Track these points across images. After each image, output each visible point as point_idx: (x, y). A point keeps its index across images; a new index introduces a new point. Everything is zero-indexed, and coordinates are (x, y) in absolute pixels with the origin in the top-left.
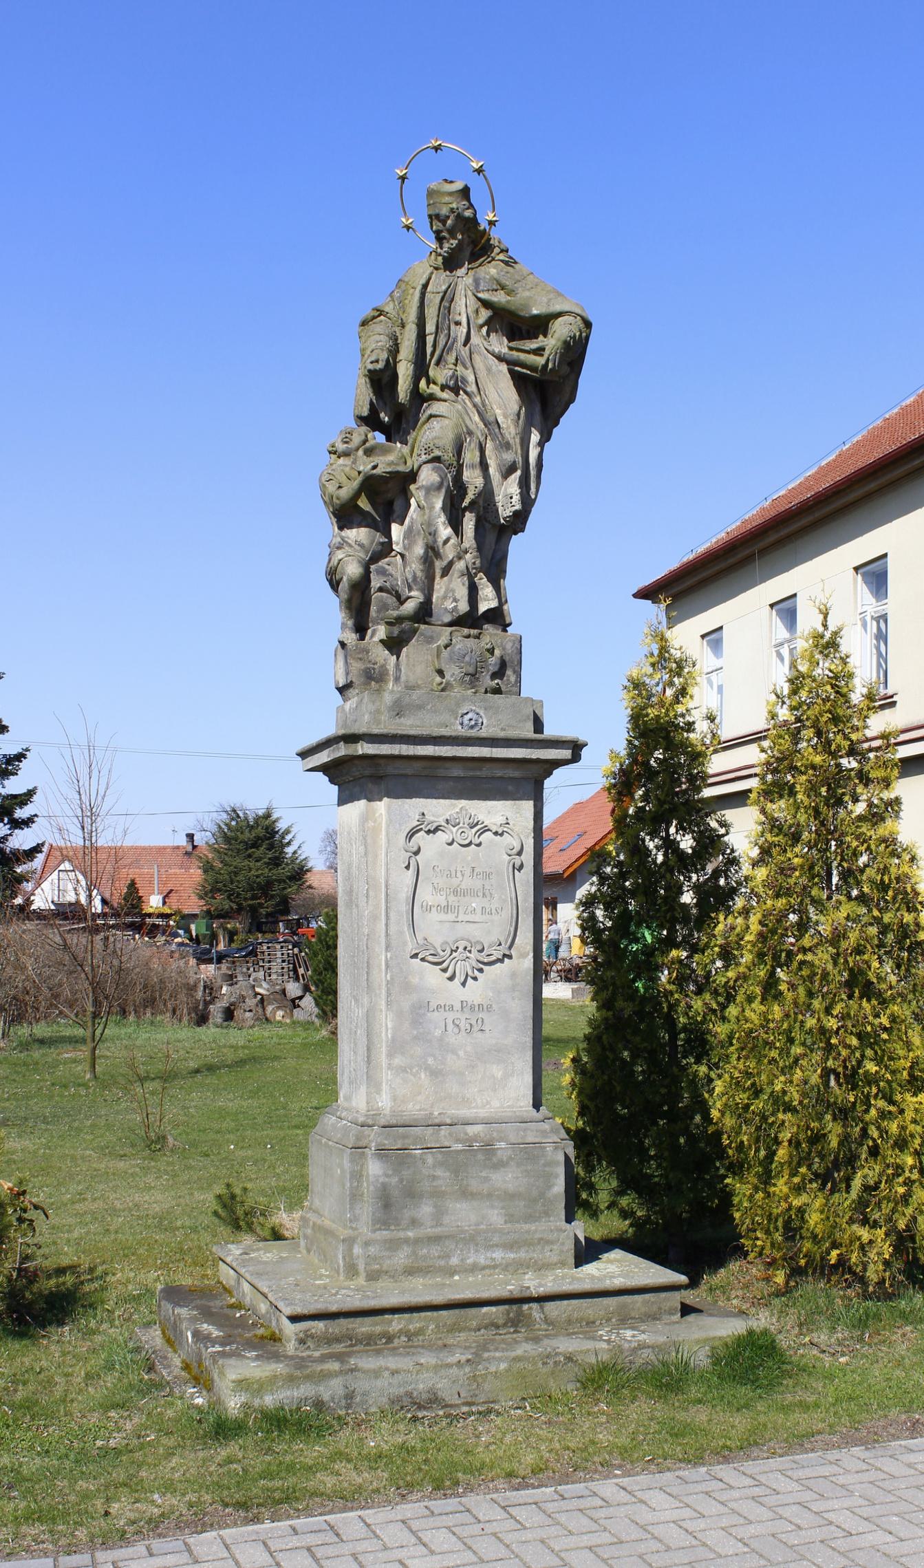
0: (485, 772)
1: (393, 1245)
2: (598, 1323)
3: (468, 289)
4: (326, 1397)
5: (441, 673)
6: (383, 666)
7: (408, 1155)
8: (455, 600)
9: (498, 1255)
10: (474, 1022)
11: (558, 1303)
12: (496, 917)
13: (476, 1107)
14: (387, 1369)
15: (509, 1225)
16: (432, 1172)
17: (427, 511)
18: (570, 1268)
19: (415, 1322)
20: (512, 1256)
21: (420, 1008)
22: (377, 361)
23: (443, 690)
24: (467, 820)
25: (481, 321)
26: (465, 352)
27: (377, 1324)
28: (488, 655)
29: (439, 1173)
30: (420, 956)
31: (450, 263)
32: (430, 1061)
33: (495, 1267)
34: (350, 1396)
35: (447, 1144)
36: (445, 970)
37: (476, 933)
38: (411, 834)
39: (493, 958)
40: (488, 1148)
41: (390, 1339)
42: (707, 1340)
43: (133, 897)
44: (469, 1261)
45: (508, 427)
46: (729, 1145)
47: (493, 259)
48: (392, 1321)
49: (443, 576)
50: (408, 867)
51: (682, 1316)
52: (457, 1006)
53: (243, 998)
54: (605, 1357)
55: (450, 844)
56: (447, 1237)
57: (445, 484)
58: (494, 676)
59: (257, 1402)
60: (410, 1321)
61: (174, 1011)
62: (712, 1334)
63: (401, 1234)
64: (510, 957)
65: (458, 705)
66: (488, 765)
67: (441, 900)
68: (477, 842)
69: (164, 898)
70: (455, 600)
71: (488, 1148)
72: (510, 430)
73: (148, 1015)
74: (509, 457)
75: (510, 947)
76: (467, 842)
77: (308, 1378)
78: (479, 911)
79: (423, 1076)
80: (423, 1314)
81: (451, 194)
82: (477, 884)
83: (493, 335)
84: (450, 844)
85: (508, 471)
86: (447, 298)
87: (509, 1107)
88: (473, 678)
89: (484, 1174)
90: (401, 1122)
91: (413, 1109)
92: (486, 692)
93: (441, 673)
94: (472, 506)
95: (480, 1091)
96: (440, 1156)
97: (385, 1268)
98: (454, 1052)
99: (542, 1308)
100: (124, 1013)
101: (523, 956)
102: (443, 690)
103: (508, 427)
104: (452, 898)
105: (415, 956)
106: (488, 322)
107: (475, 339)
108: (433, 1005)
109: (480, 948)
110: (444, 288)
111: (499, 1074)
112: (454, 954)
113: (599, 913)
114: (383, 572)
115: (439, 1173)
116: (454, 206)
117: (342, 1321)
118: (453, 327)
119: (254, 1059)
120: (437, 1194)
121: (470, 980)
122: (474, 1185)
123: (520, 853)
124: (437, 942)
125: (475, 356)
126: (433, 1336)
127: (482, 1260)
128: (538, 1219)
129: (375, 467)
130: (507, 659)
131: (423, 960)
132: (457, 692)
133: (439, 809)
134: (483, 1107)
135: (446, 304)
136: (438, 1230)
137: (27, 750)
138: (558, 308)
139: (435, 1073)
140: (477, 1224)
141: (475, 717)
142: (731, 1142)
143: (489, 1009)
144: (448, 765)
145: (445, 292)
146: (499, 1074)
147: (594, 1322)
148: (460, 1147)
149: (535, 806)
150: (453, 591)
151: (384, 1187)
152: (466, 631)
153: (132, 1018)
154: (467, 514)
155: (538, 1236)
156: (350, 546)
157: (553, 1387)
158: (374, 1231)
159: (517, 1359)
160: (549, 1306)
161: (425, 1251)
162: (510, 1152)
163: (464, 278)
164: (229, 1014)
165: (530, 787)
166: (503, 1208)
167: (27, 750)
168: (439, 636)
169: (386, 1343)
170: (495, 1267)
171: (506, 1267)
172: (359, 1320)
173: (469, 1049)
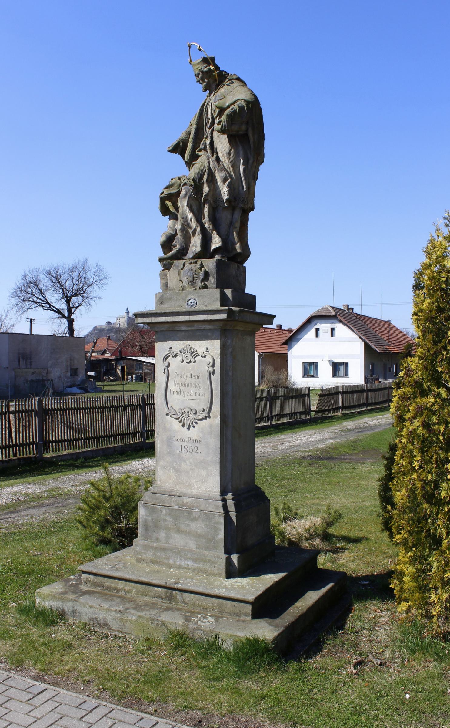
0: (196, 327)
2: (208, 610)
7: (156, 507)
9: (190, 563)
10: (193, 448)
12: (202, 398)
14: (88, 604)
15: (198, 550)
18: (223, 578)
19: (129, 586)
20: (197, 565)
21: (171, 439)
23: (183, 290)
27: (113, 583)
28: (200, 271)
30: (170, 415)
32: (175, 464)
33: (189, 569)
35: (173, 505)
37: (193, 405)
42: (232, 636)
47: (224, 85)
48: (118, 583)
49: (193, 236)
50: (164, 372)
52: (186, 440)
55: (182, 362)
57: (189, 194)
60: (126, 585)
62: (235, 634)
63: (151, 544)
64: (209, 417)
65: (186, 296)
66: (196, 324)
72: (225, 161)
75: (209, 412)
77: (60, 599)
78: (194, 394)
80: (131, 583)
81: (198, 64)
84: (182, 362)
88: (192, 282)
90: (159, 492)
95: (196, 482)
96: (168, 511)
97: (143, 558)
99: (182, 595)
101: (215, 417)
104: (182, 388)
105: (167, 414)
108: (176, 438)
109: (194, 412)
111: (205, 475)
112: (184, 415)
115: (168, 518)
117: (99, 577)
120: (167, 529)
121: (191, 428)
122: (183, 527)
123: (213, 366)
124: (177, 408)
130: (210, 272)
139: (177, 471)
140: (184, 546)
143: (200, 441)
144: (179, 325)
146: (205, 475)
147: (206, 609)
148: (177, 507)
151: (146, 520)
154: (205, 205)
155: (208, 558)
158: (142, 540)
159: (139, 617)
160: (185, 595)
161: (159, 554)
162: (199, 514)
165: (218, 333)
169: (116, 593)
170: (189, 569)
172: (106, 579)
173: (191, 461)
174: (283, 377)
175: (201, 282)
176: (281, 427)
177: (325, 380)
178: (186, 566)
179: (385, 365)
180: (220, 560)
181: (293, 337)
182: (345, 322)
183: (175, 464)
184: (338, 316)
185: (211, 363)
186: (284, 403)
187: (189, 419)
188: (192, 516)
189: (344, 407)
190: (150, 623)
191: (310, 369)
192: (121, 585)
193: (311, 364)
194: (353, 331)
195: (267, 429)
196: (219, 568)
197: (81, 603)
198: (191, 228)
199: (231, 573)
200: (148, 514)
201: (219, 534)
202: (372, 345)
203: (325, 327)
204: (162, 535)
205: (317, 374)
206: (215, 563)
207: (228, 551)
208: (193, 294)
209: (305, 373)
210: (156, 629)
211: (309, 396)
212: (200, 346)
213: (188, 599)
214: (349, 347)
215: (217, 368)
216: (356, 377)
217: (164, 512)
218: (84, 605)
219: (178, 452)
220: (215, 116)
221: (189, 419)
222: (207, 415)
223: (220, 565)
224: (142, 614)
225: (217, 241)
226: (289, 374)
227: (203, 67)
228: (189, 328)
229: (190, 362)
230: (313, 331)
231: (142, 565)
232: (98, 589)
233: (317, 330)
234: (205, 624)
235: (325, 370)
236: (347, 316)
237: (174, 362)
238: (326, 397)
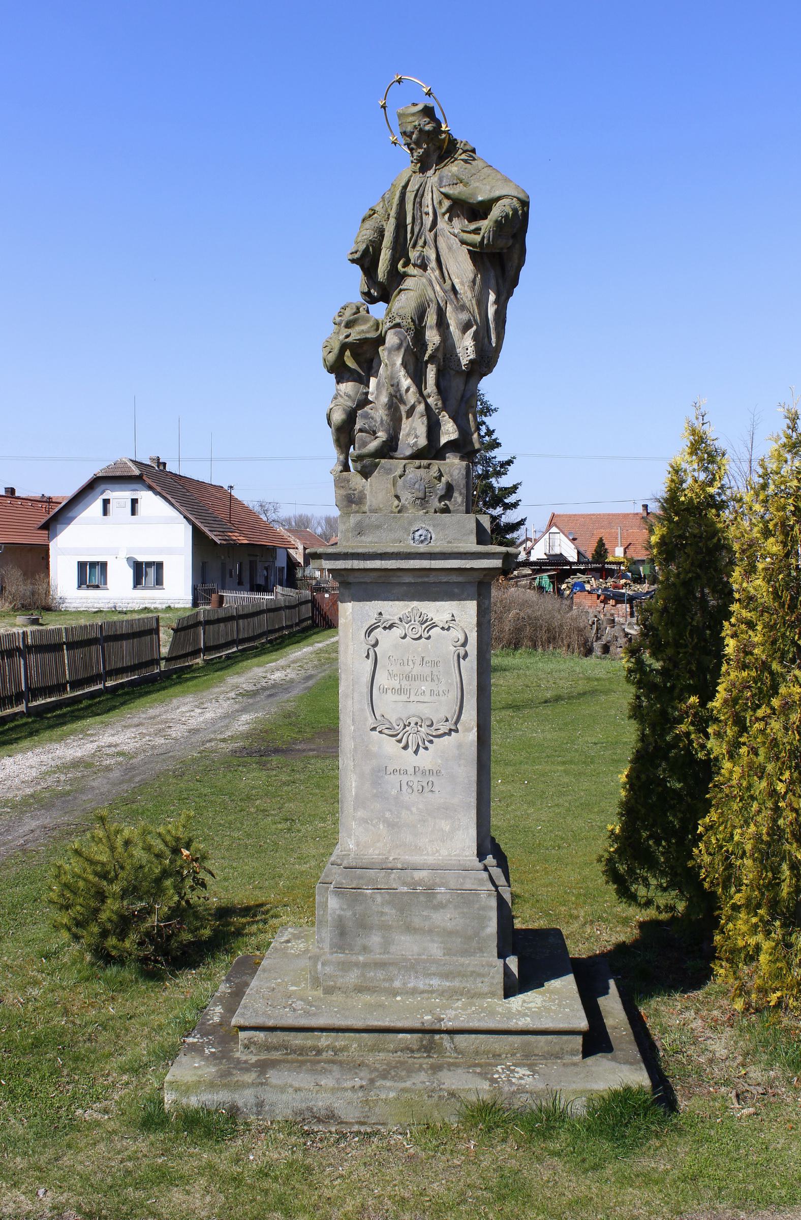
0: (432, 579)
1: (345, 967)
2: (504, 1056)
3: (436, 184)
4: (240, 1104)
5: (397, 497)
6: (362, 492)
8: (416, 437)
9: (435, 982)
10: (425, 784)
11: (467, 1036)
13: (428, 854)
14: (291, 1086)
15: (447, 957)
16: (380, 909)
17: (389, 368)
18: (500, 999)
19: (341, 1040)
20: (448, 984)
21: (379, 771)
22: (356, 252)
23: (399, 512)
24: (417, 618)
25: (443, 210)
26: (430, 236)
27: (308, 1039)
28: (437, 482)
29: (386, 910)
31: (424, 165)
32: (388, 815)
33: (432, 992)
34: (260, 1105)
35: (394, 886)
36: (400, 741)
37: (426, 711)
38: (370, 631)
39: (440, 732)
40: (430, 891)
41: (319, 1052)
42: (583, 1092)
43: (601, 551)
44: (410, 985)
45: (465, 292)
46: (704, 879)
47: (456, 159)
48: (320, 1038)
49: (408, 417)
50: (368, 657)
51: (584, 1057)
53: (616, 638)
54: (486, 1097)
55: (404, 637)
56: (391, 964)
57: (405, 345)
58: (441, 499)
59: (184, 1101)
60: (336, 1039)
61: (569, 646)
64: (457, 731)
66: (434, 573)
67: (395, 683)
68: (427, 635)
69: (625, 549)
70: (416, 437)
71: (430, 891)
72: (467, 295)
73: (551, 648)
74: (464, 316)
75: (456, 723)
76: (417, 636)
77: (226, 1086)
78: (428, 693)
79: (381, 827)
80: (347, 1035)
81: (413, 114)
82: (426, 670)
83: (455, 220)
84: (404, 637)
85: (466, 327)
86: (419, 195)
87: (455, 855)
88: (423, 501)
89: (425, 913)
90: (360, 865)
91: (374, 853)
92: (436, 512)
93: (397, 497)
94: (432, 358)
95: (430, 841)
96: (387, 897)
97: (338, 985)
98: (408, 808)
99: (452, 1039)
100: (535, 647)
101: (469, 730)
102: (399, 512)
103: (465, 292)
104: (405, 683)
105: (374, 729)
106: (449, 210)
107: (442, 224)
109: (429, 723)
110: (417, 187)
111: (447, 828)
112: (407, 728)
113: (646, 656)
114: (366, 416)
115: (386, 910)
116: (417, 123)
117: (279, 1033)
118: (424, 216)
119: (593, 692)
120: (385, 928)
121: (421, 750)
122: (417, 922)
123: (464, 645)
125: (440, 239)
126: (356, 1054)
127: (421, 985)
128: (473, 954)
129: (347, 336)
130: (454, 484)
131: (380, 732)
132: (411, 513)
133: (393, 609)
134: (433, 854)
135: (418, 200)
136: (385, 957)
137: (514, 458)
138: (497, 193)
139: (392, 825)
141: (424, 533)
142: (707, 876)
143: (438, 773)
145: (418, 190)
147: (500, 1055)
148: (405, 889)
149: (479, 606)
150: (415, 429)
151: (340, 919)
152: (417, 462)
153: (540, 650)
154: (429, 365)
155: (470, 969)
156: (341, 397)
157: (437, 1119)
158: (332, 953)
159: (404, 1090)
160: (458, 1038)
161: (372, 974)
162: (448, 896)
163: (432, 178)
164: (606, 649)
165: (473, 590)
166: (441, 943)
167: (514, 458)
168: (396, 467)
169: (316, 1055)
170: (432, 992)
171: (442, 993)
172: (293, 1034)
173: (421, 806)
174: (41, 589)
175: (440, 500)
176: (120, 692)
177: (120, 593)
178: (427, 988)
179: (223, 565)
180: (493, 970)
181: (58, 515)
182: (159, 489)
183: (388, 815)
184: (144, 478)
185: (462, 640)
186: (122, 647)
187: (412, 734)
188: (435, 902)
189: (208, 649)
190: (425, 1097)
191: (91, 573)
192: (327, 1040)
193: (93, 565)
194: (172, 505)
195: (100, 696)
196: (492, 984)
197: (275, 1086)
198: (405, 404)
199: (512, 988)
200: (345, 907)
201: (487, 926)
202: (206, 530)
203: (120, 497)
204: (375, 939)
205: (105, 583)
206: (483, 976)
207: (502, 955)
208: (424, 522)
209: (82, 582)
210: (437, 1105)
211: (157, 631)
212: (439, 611)
213: (465, 1044)
214: (166, 535)
215: (472, 648)
216: (177, 590)
217: (379, 899)
218: (282, 1089)
219: (394, 792)
220: (440, 211)
221: (412, 734)
222: (453, 728)
223: (493, 977)
224: (402, 1085)
225: (451, 430)
226: (52, 582)
227: (422, 123)
228: (420, 580)
229: (420, 637)
230: (98, 505)
231: (337, 998)
232: (276, 1055)
233: (106, 502)
234: (523, 1081)
235: (120, 576)
236: (153, 477)
237: (387, 640)
238: (183, 633)
